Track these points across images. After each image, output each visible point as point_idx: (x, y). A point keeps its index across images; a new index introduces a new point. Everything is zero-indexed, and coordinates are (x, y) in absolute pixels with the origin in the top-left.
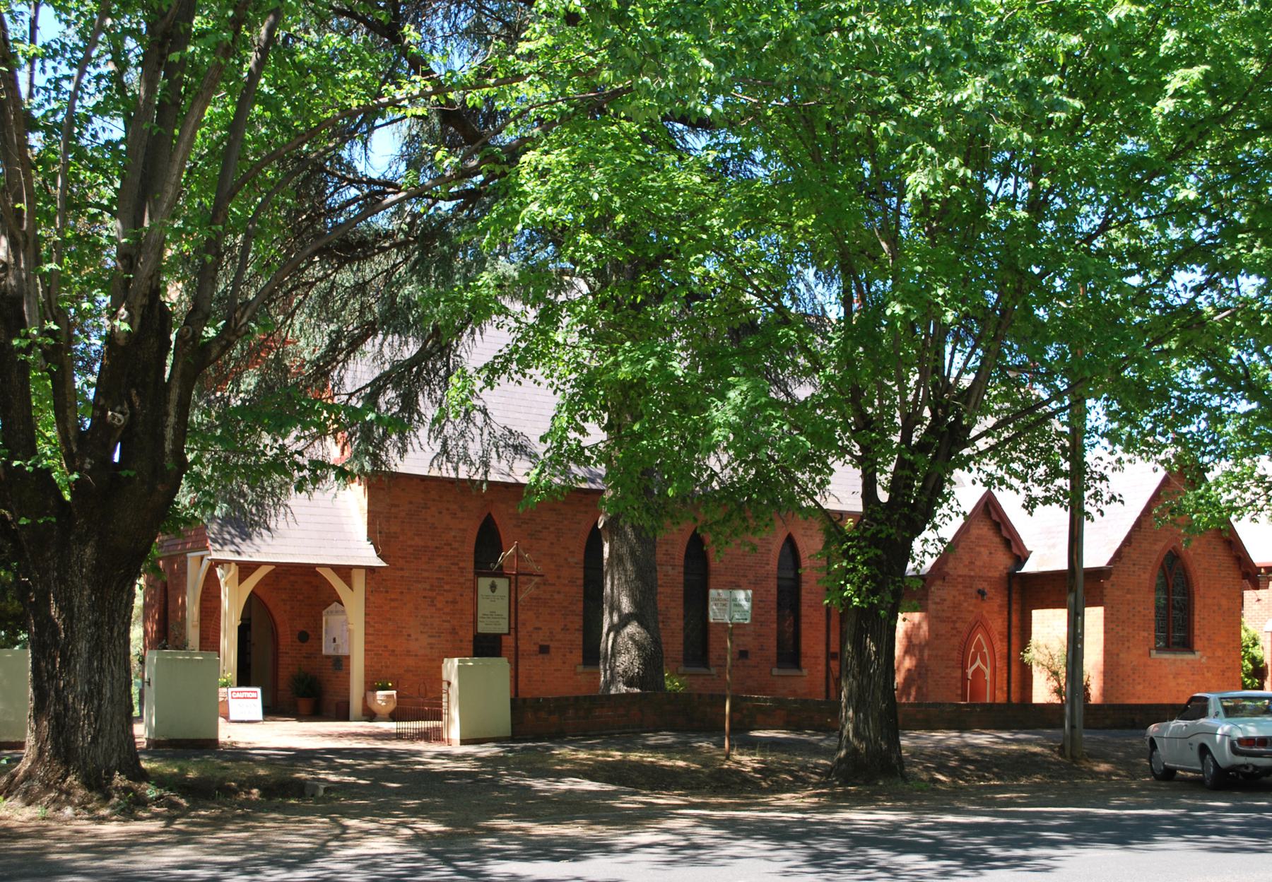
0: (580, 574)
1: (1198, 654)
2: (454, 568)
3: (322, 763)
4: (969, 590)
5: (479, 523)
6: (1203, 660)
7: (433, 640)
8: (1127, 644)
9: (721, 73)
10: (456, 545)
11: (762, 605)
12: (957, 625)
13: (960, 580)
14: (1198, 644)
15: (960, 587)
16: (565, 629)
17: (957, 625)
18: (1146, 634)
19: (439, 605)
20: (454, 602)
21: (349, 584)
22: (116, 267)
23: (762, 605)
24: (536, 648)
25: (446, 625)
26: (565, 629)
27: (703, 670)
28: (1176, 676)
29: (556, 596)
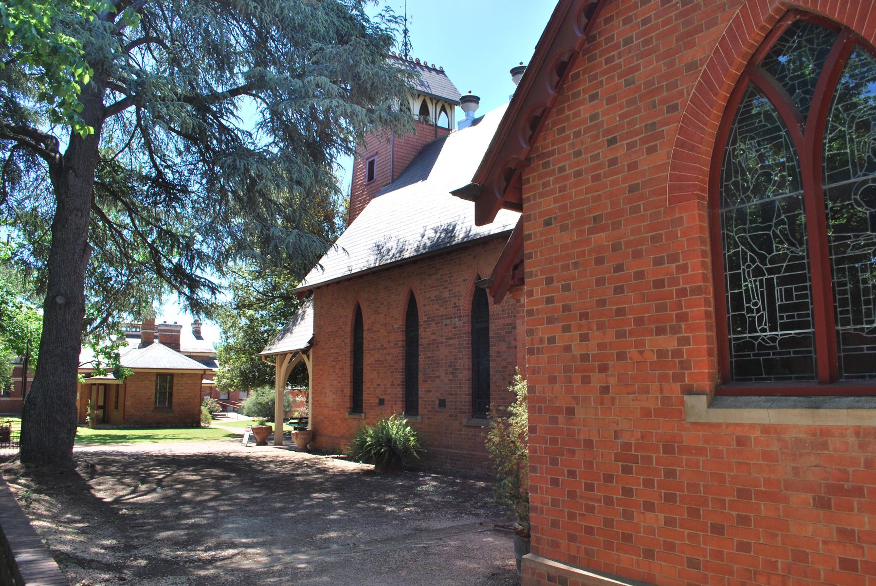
8: (597, 379)
24: (377, 401)
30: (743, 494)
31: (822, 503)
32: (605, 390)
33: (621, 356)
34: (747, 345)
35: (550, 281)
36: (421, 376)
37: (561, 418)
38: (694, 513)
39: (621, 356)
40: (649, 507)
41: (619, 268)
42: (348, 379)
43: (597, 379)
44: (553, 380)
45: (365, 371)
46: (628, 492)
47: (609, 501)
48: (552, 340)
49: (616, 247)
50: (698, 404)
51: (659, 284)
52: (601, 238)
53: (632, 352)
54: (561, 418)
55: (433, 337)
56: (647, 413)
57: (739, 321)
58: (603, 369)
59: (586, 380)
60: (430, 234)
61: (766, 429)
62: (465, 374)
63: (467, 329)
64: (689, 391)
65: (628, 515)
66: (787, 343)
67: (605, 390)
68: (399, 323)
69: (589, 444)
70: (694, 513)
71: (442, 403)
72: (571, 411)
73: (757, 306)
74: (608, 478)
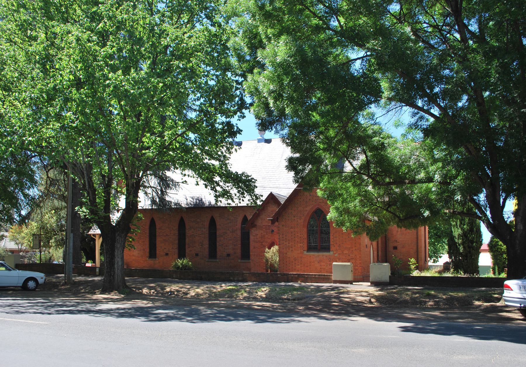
0: (177, 232)
1: (331, 253)
2: (144, 233)
3: (322, 303)
4: (268, 231)
5: (209, 219)
6: (336, 255)
7: (139, 252)
8: (291, 249)
9: (344, 91)
10: (144, 226)
11: (235, 239)
12: (263, 244)
13: (264, 227)
14: (332, 248)
15: (264, 230)
16: (173, 248)
17: (263, 244)
18: (302, 245)
19: (140, 243)
20: (144, 242)
21: (95, 237)
22: (145, 174)
23: (235, 239)
24: (165, 254)
25: (142, 248)
26: (173, 248)
27: (214, 260)
28: (319, 262)
29: (170, 239)
30: (310, 262)
31: (318, 262)
32: (292, 250)
33: (295, 246)
34: (311, 246)
35: (283, 234)
36: (187, 246)
37: (285, 254)
38: (304, 265)
39: (295, 246)
40: (298, 265)
41: (295, 234)
42: (147, 246)
43: (291, 249)
44: (283, 249)
45: (157, 243)
46: (295, 263)
47: (292, 265)
48: (283, 243)
49: (294, 231)
50: (305, 252)
51: (300, 237)
52: (292, 230)
53: (296, 246)
54: (285, 254)
55: (193, 233)
56: (298, 253)
57: (310, 243)
58: (292, 248)
59: (289, 249)
60: (190, 199)
61: (313, 255)
62: (206, 246)
63: (208, 232)
64: (304, 251)
65: (295, 266)
66: (315, 245)
67: (292, 250)
68: (206, 231)
69: (289, 258)
70: (304, 265)
71: (197, 255)
72: (286, 253)
73: (312, 241)
74: (292, 262)
